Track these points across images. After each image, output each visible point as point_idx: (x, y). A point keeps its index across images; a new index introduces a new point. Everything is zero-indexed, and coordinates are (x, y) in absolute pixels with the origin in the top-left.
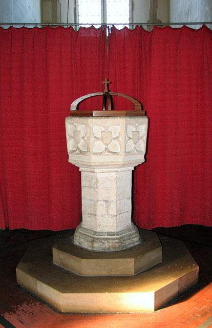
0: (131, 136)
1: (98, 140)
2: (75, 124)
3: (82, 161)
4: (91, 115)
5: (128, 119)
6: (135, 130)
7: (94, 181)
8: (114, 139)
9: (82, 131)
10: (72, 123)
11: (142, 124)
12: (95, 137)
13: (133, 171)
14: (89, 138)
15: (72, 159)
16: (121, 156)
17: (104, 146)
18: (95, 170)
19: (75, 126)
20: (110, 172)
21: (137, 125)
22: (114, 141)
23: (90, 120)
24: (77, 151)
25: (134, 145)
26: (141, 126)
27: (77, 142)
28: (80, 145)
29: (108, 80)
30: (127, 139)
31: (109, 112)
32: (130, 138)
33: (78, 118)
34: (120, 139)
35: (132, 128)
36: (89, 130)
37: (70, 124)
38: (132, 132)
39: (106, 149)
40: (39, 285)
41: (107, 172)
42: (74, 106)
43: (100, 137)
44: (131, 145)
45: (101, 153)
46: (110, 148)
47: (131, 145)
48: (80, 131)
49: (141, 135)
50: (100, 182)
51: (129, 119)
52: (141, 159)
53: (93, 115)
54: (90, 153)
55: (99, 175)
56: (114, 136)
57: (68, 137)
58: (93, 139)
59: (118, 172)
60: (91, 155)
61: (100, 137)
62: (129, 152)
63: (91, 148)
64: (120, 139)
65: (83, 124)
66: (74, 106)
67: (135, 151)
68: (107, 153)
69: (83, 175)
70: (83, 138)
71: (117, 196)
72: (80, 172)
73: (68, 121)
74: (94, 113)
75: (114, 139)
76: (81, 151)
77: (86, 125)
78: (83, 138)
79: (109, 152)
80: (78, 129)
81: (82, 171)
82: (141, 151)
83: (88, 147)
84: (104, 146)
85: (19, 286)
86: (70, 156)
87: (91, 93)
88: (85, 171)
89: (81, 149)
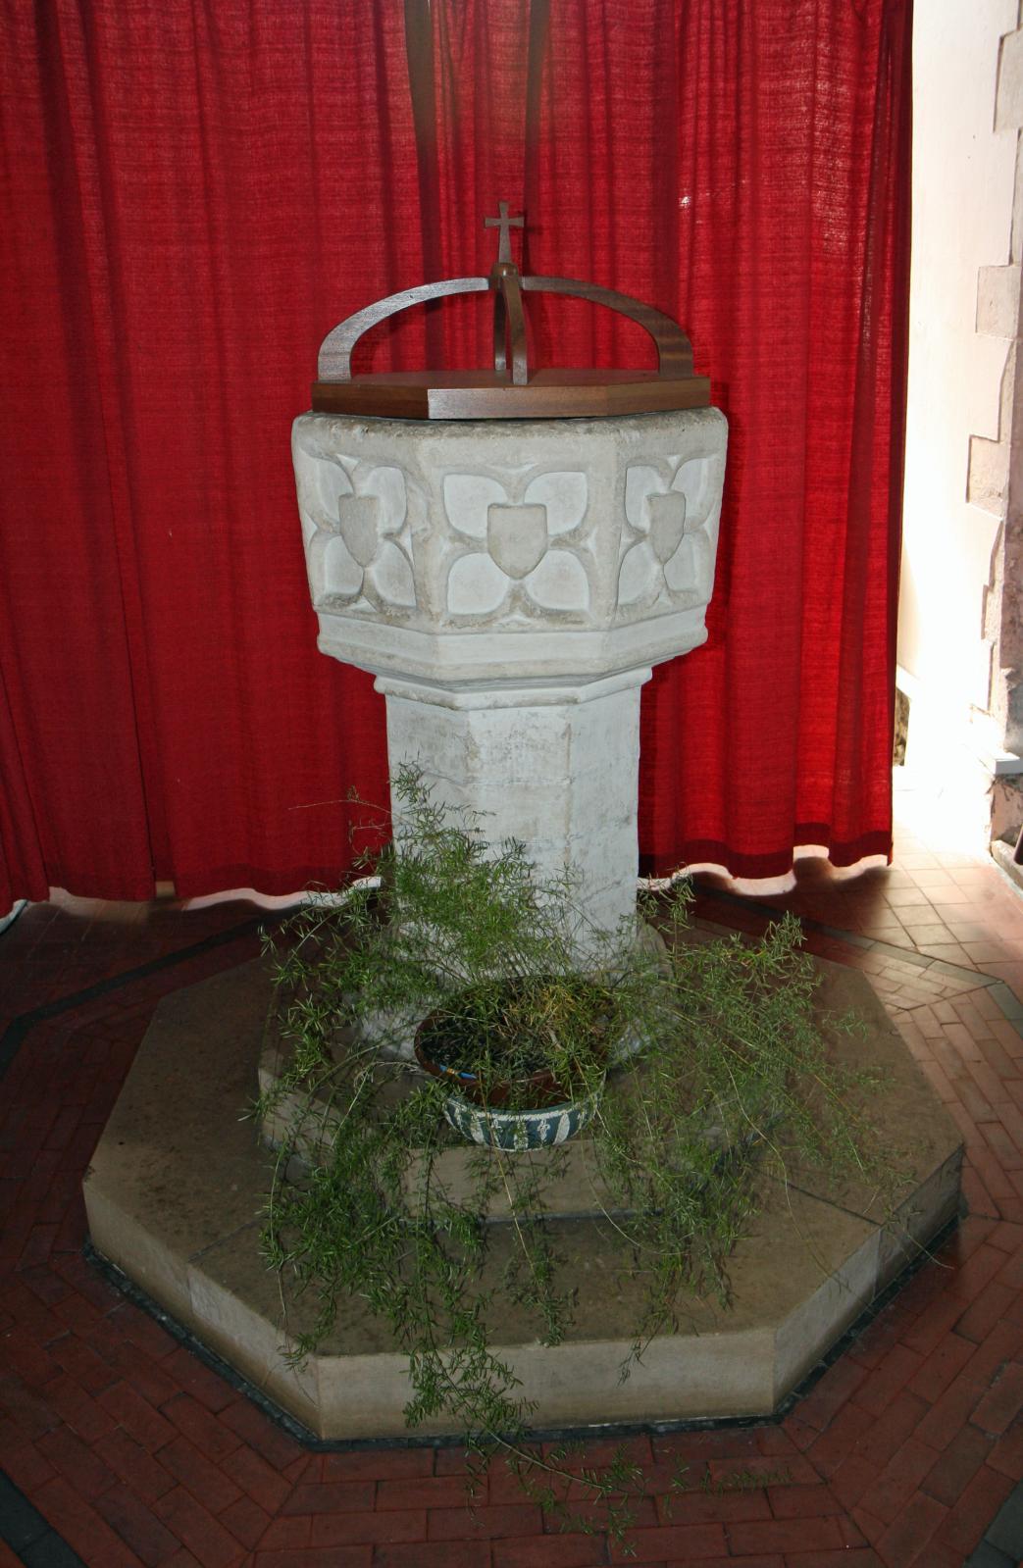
0: (645, 524)
1: (474, 550)
2: (344, 459)
3: (390, 657)
4: (415, 413)
5: (633, 434)
6: (662, 490)
7: (453, 750)
8: (560, 542)
9: (384, 503)
10: (330, 456)
11: (699, 453)
12: (459, 537)
13: (647, 689)
14: (421, 544)
15: (336, 639)
16: (597, 629)
17: (506, 583)
18: (461, 699)
19: (345, 470)
20: (534, 704)
21: (673, 460)
22: (554, 556)
23: (429, 448)
24: (364, 604)
25: (655, 567)
26: (429, 391)
27: (360, 556)
28: (373, 572)
29: (331, 1001)
30: (626, 540)
31: (518, 392)
32: (639, 536)
33: (357, 430)
34: (590, 543)
35: (647, 483)
36: (420, 502)
37: (319, 456)
38: (650, 499)
39: (516, 597)
40: (197, 1287)
41: (518, 705)
42: (335, 356)
43: (480, 532)
44: (644, 576)
45: (489, 619)
46: (535, 588)
47: (644, 576)
48: (372, 499)
49: (691, 511)
50: (483, 755)
51: (636, 435)
52: (690, 631)
53: (432, 414)
54: (433, 617)
55: (474, 718)
56: (559, 526)
57: (309, 527)
58: (447, 546)
59: (575, 702)
60: (439, 626)
61: (480, 532)
62: (631, 606)
63: (434, 587)
64: (590, 543)
65: (387, 462)
66: (335, 356)
67: (664, 599)
68: (518, 616)
69: (393, 709)
70: (389, 536)
71: (569, 819)
72: (381, 699)
73: (309, 440)
74: (438, 401)
75: (560, 542)
76: (380, 602)
77: (404, 469)
78: (389, 536)
79: (530, 612)
80: (364, 488)
81: (392, 693)
82: (689, 592)
83: (419, 589)
84: (506, 583)
85: (105, 1268)
86: (325, 621)
87: (428, 281)
88: (406, 697)
89: (381, 592)
